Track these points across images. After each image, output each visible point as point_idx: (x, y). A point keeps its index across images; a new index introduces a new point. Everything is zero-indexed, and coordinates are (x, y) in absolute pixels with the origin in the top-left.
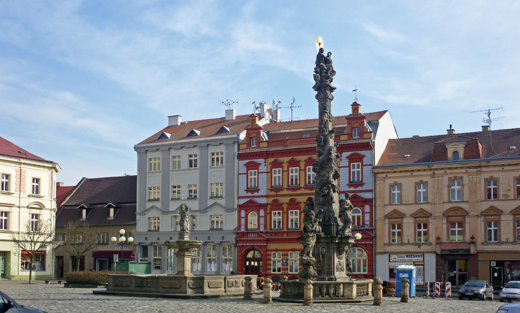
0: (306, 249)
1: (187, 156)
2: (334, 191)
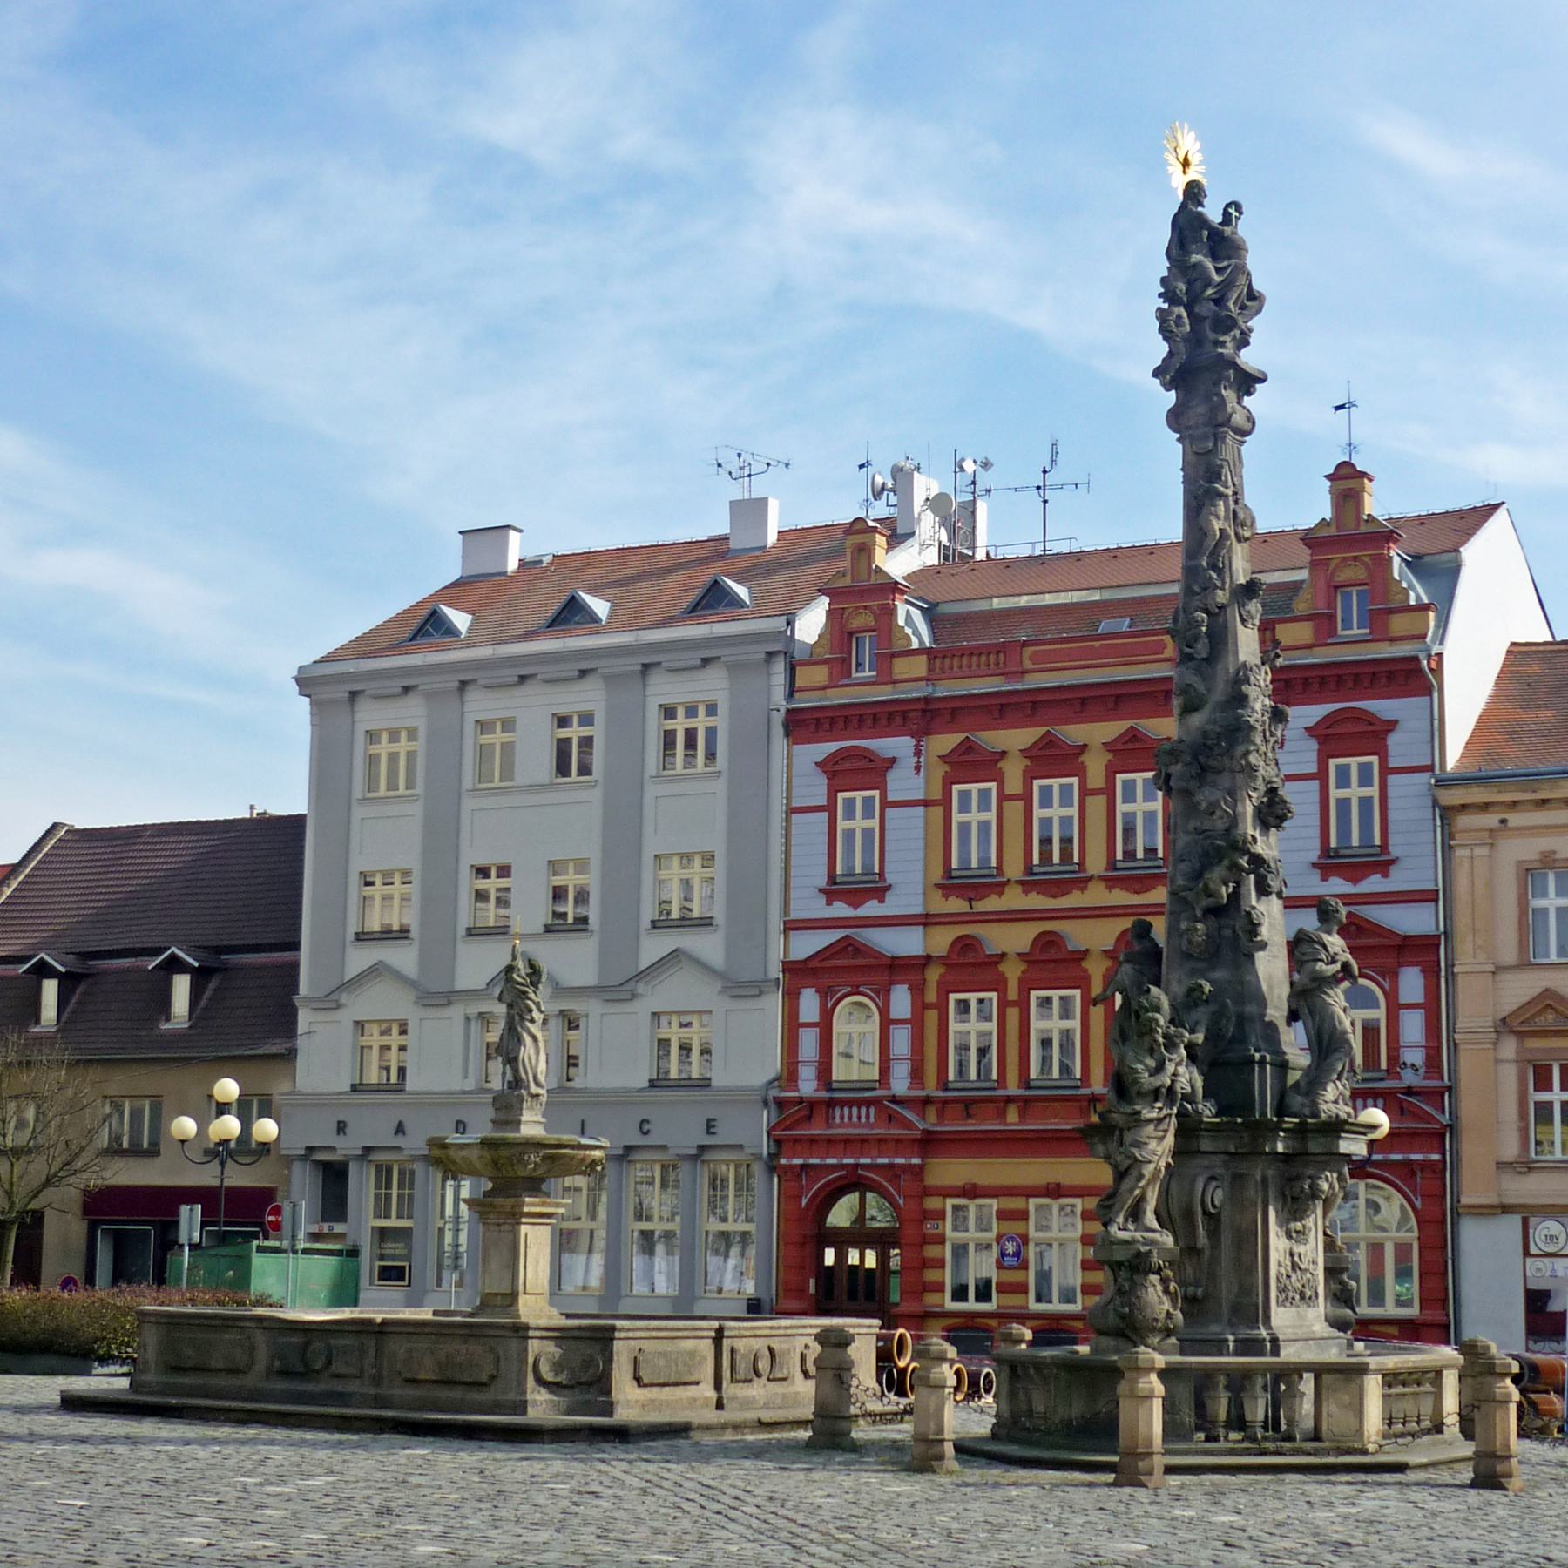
0: (1126, 1185)
1: (547, 723)
2: (1263, 890)
